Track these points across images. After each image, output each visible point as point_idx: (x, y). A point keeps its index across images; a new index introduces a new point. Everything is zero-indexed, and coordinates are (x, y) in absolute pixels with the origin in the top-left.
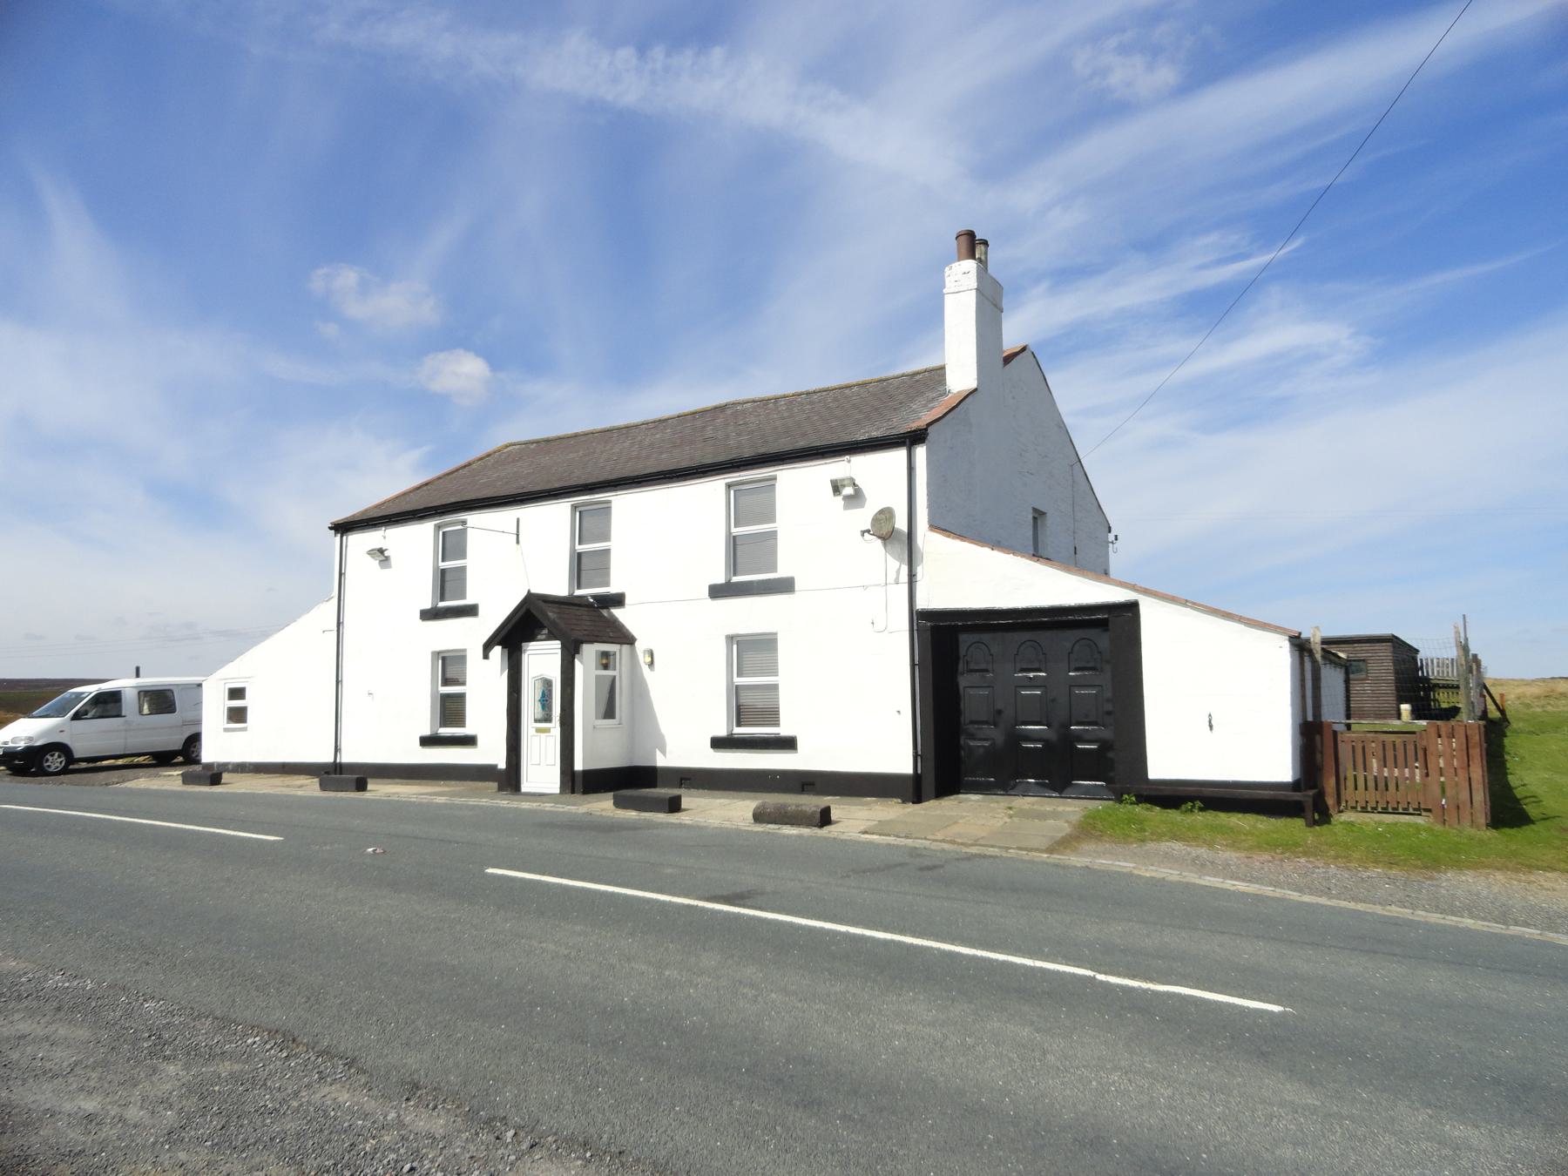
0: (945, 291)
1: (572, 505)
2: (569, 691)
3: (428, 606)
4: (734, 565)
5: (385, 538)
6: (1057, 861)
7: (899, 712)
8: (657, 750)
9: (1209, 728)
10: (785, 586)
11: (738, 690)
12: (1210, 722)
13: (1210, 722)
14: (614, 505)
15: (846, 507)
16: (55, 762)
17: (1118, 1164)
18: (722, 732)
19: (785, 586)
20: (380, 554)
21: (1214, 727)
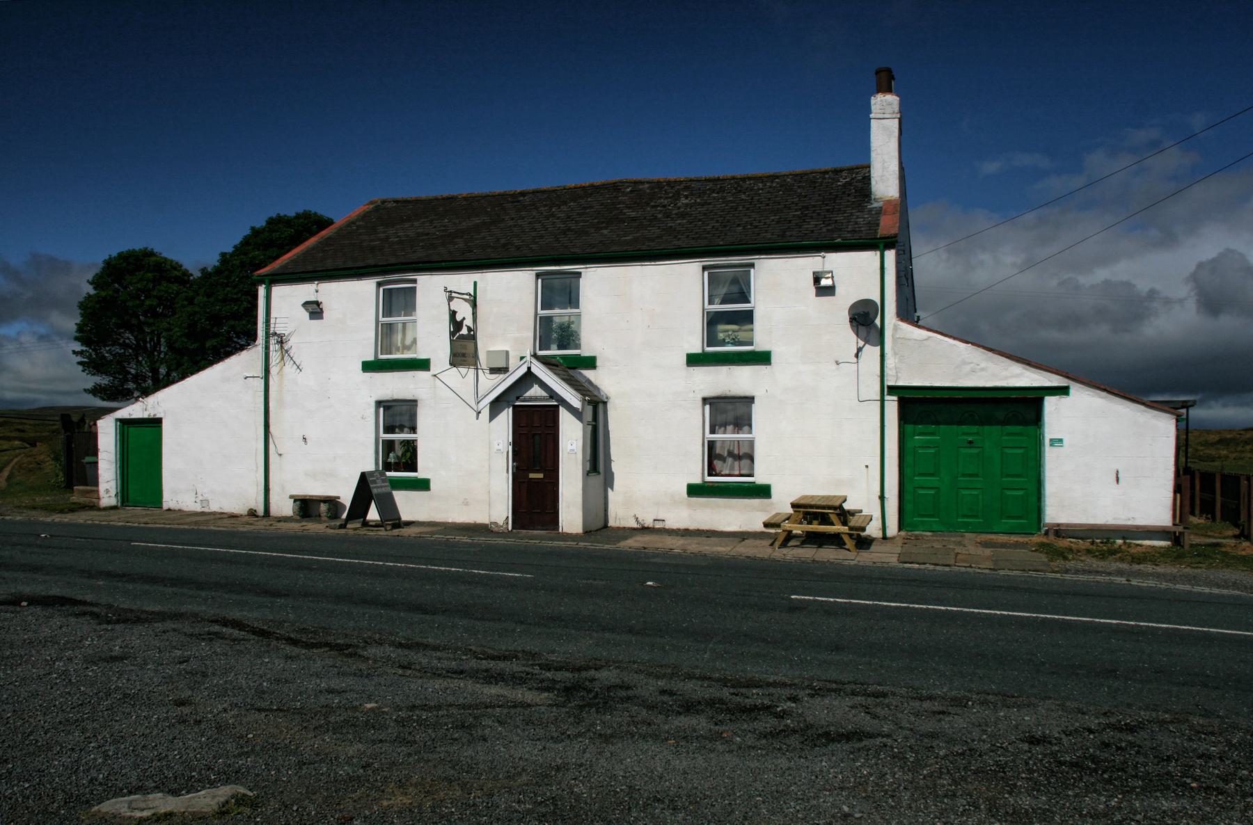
0: (872, 116)
1: (536, 274)
2: (901, 430)
3: (371, 358)
4: (711, 339)
5: (317, 291)
6: (1201, 572)
7: (867, 466)
8: (373, 504)
9: (1116, 482)
10: (763, 358)
11: (711, 445)
12: (1117, 475)
13: (1117, 475)
14: (419, 286)
15: (311, 318)
16: (597, 480)
17: (931, 777)
18: (697, 480)
19: (763, 358)
20: (315, 310)
21: (1120, 480)
